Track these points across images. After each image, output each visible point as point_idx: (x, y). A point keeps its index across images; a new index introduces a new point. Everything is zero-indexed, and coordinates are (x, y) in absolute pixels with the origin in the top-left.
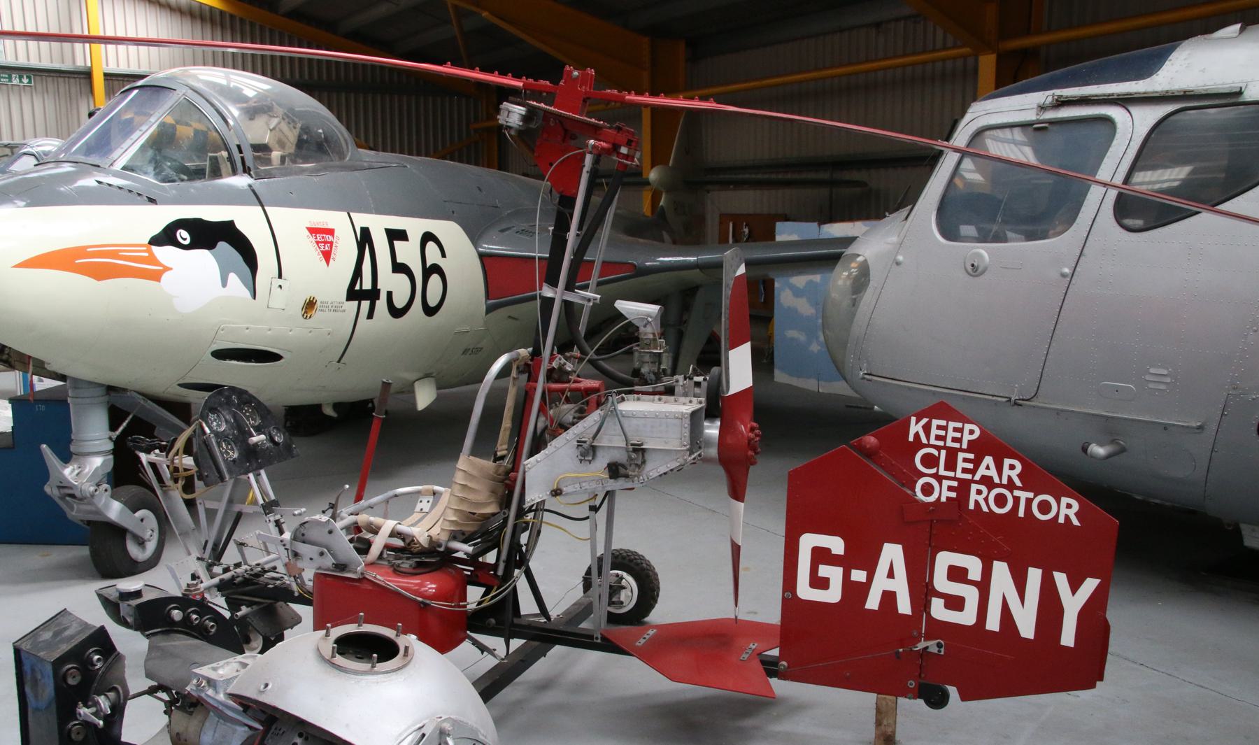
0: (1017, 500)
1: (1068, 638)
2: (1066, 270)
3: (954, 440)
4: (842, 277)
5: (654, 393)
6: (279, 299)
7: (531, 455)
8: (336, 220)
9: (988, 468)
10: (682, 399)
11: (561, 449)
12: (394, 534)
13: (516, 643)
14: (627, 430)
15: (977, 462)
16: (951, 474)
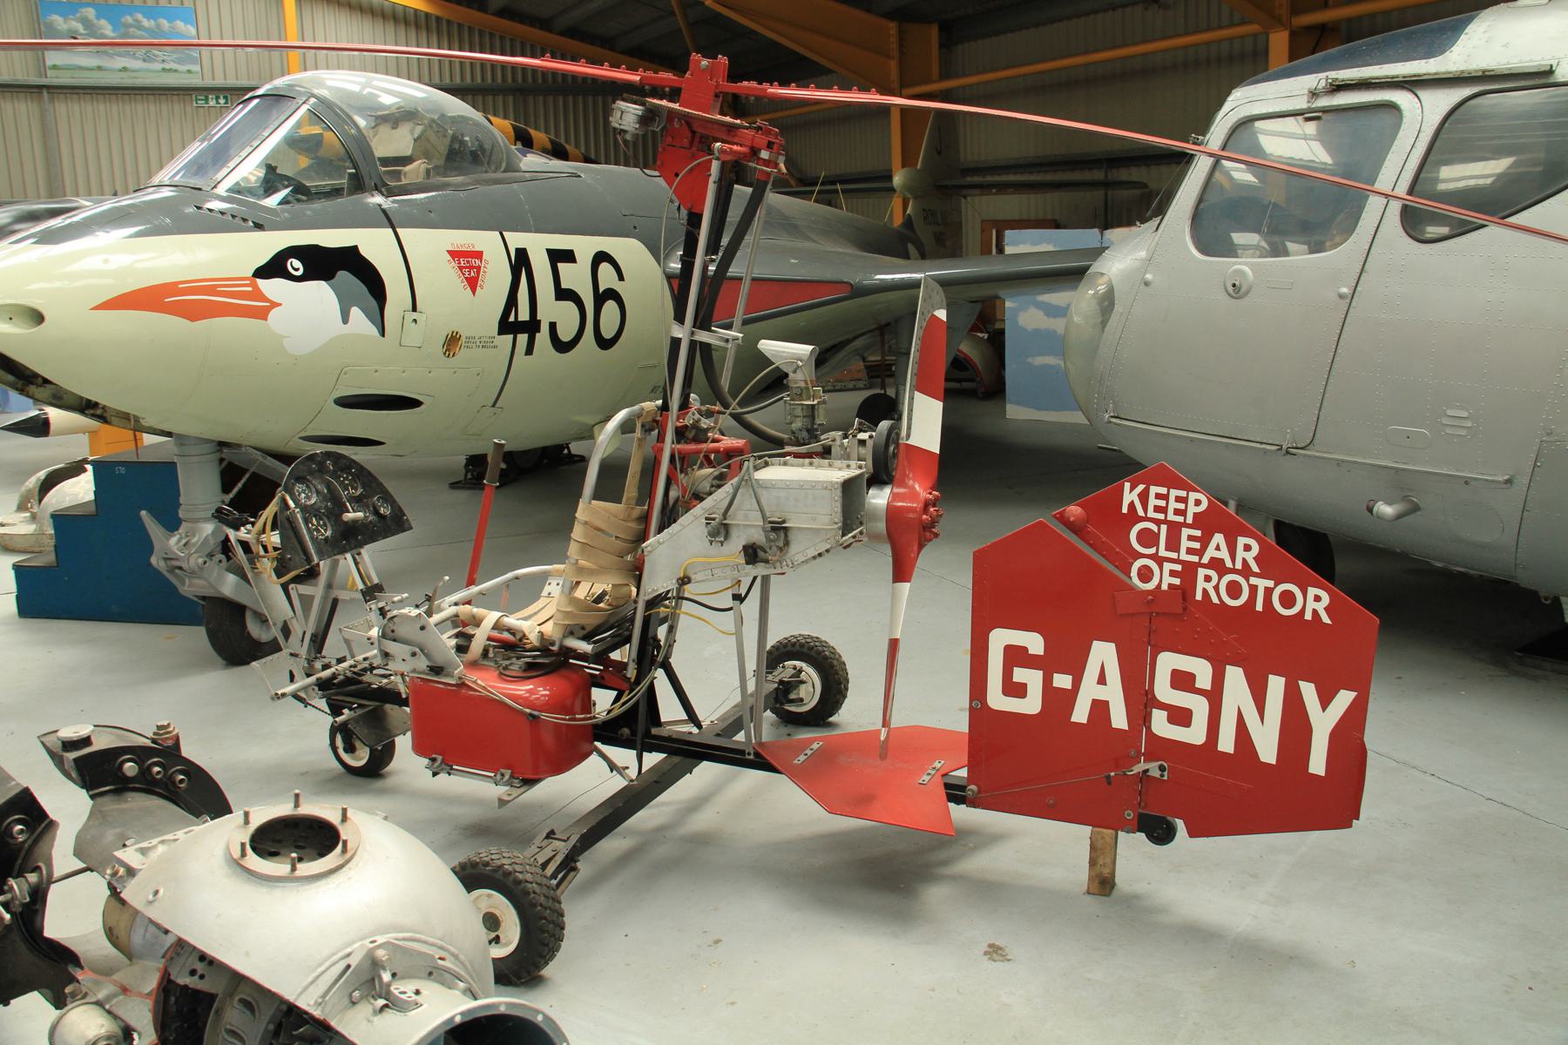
0: (1253, 589)
1: (1318, 764)
2: (1344, 290)
3: (1177, 512)
4: (1081, 301)
5: (809, 455)
6: (414, 335)
7: (660, 530)
8: (487, 242)
9: (1218, 548)
10: (838, 463)
11: (691, 525)
12: (497, 626)
13: (652, 759)
14: (764, 503)
15: (1205, 541)
16: (1174, 555)
